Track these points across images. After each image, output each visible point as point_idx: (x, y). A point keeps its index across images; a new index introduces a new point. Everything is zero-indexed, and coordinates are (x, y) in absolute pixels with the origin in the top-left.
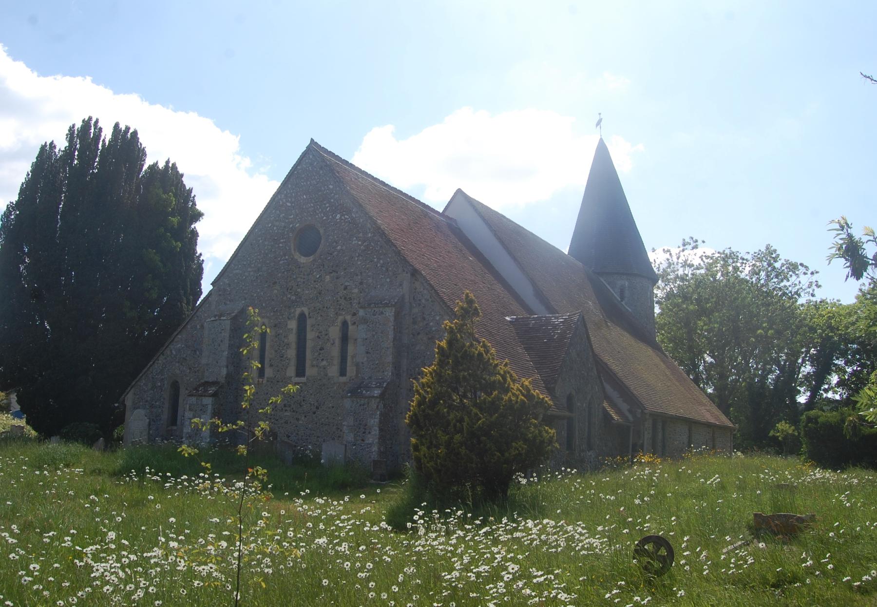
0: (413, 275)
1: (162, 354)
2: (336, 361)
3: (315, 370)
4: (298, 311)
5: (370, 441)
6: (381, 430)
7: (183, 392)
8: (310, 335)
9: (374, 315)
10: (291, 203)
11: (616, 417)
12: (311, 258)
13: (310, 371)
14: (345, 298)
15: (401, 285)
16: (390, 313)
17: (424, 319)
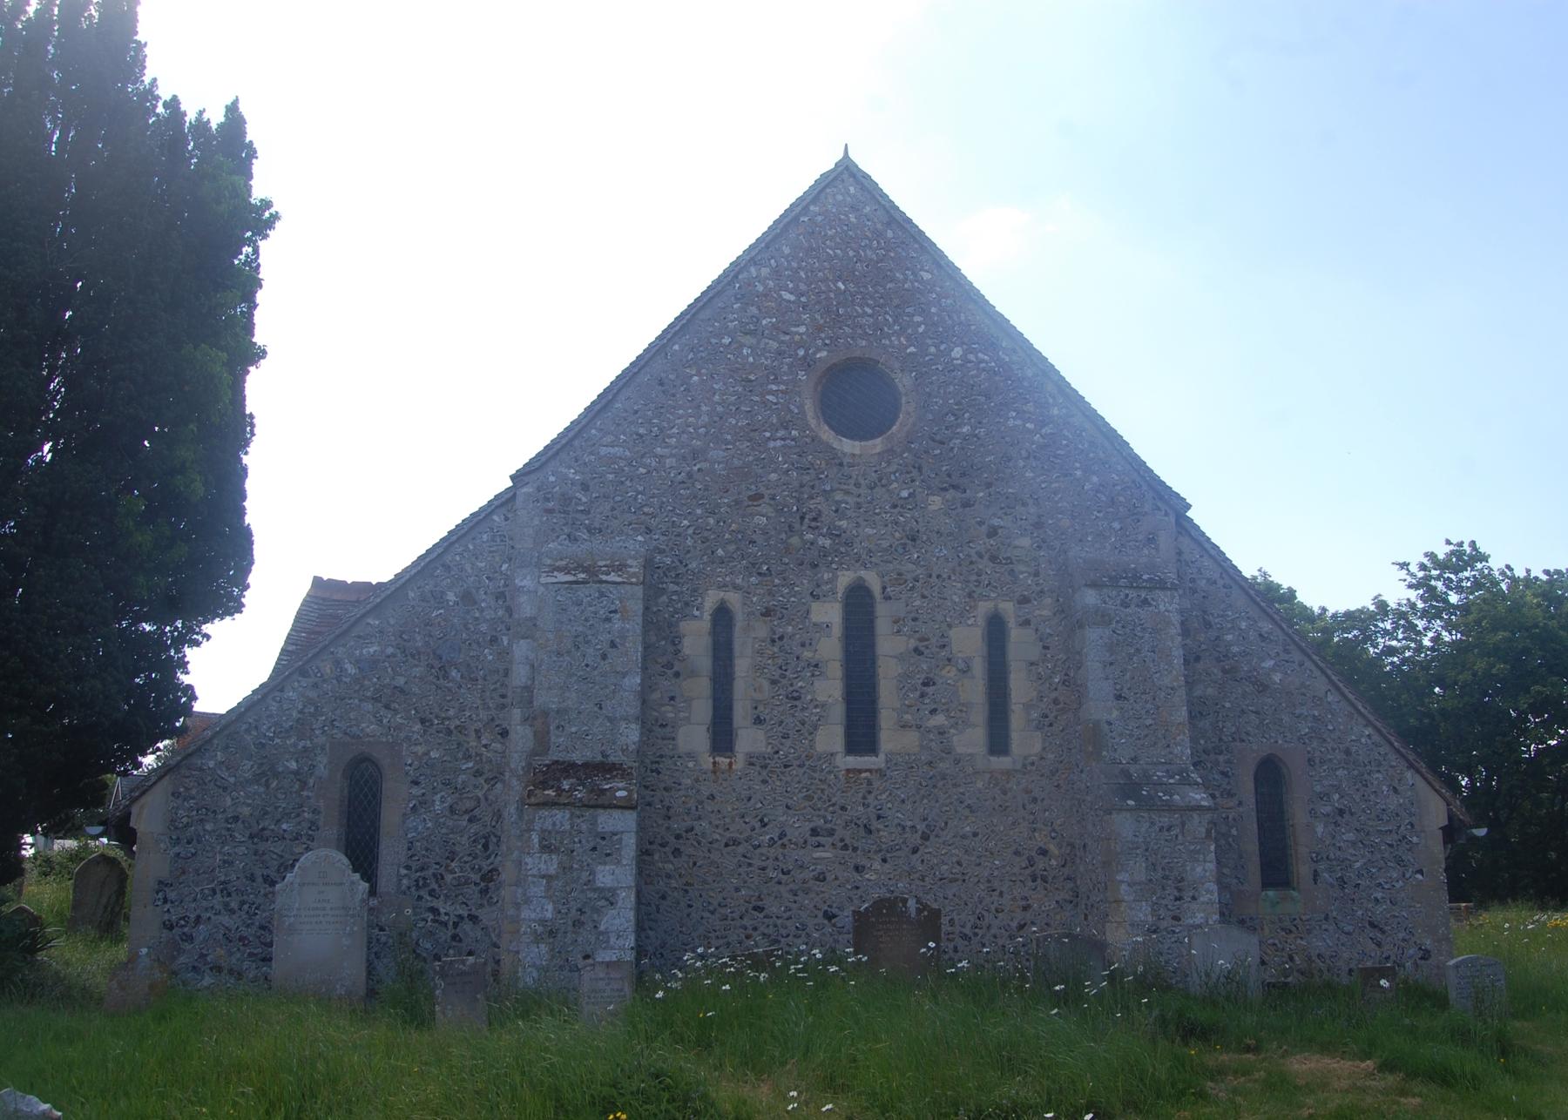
2: (979, 716)
3: (911, 740)
4: (845, 579)
5: (1199, 918)
8: (889, 646)
9: (1125, 605)
12: (878, 444)
13: (890, 739)
17: (1208, 625)
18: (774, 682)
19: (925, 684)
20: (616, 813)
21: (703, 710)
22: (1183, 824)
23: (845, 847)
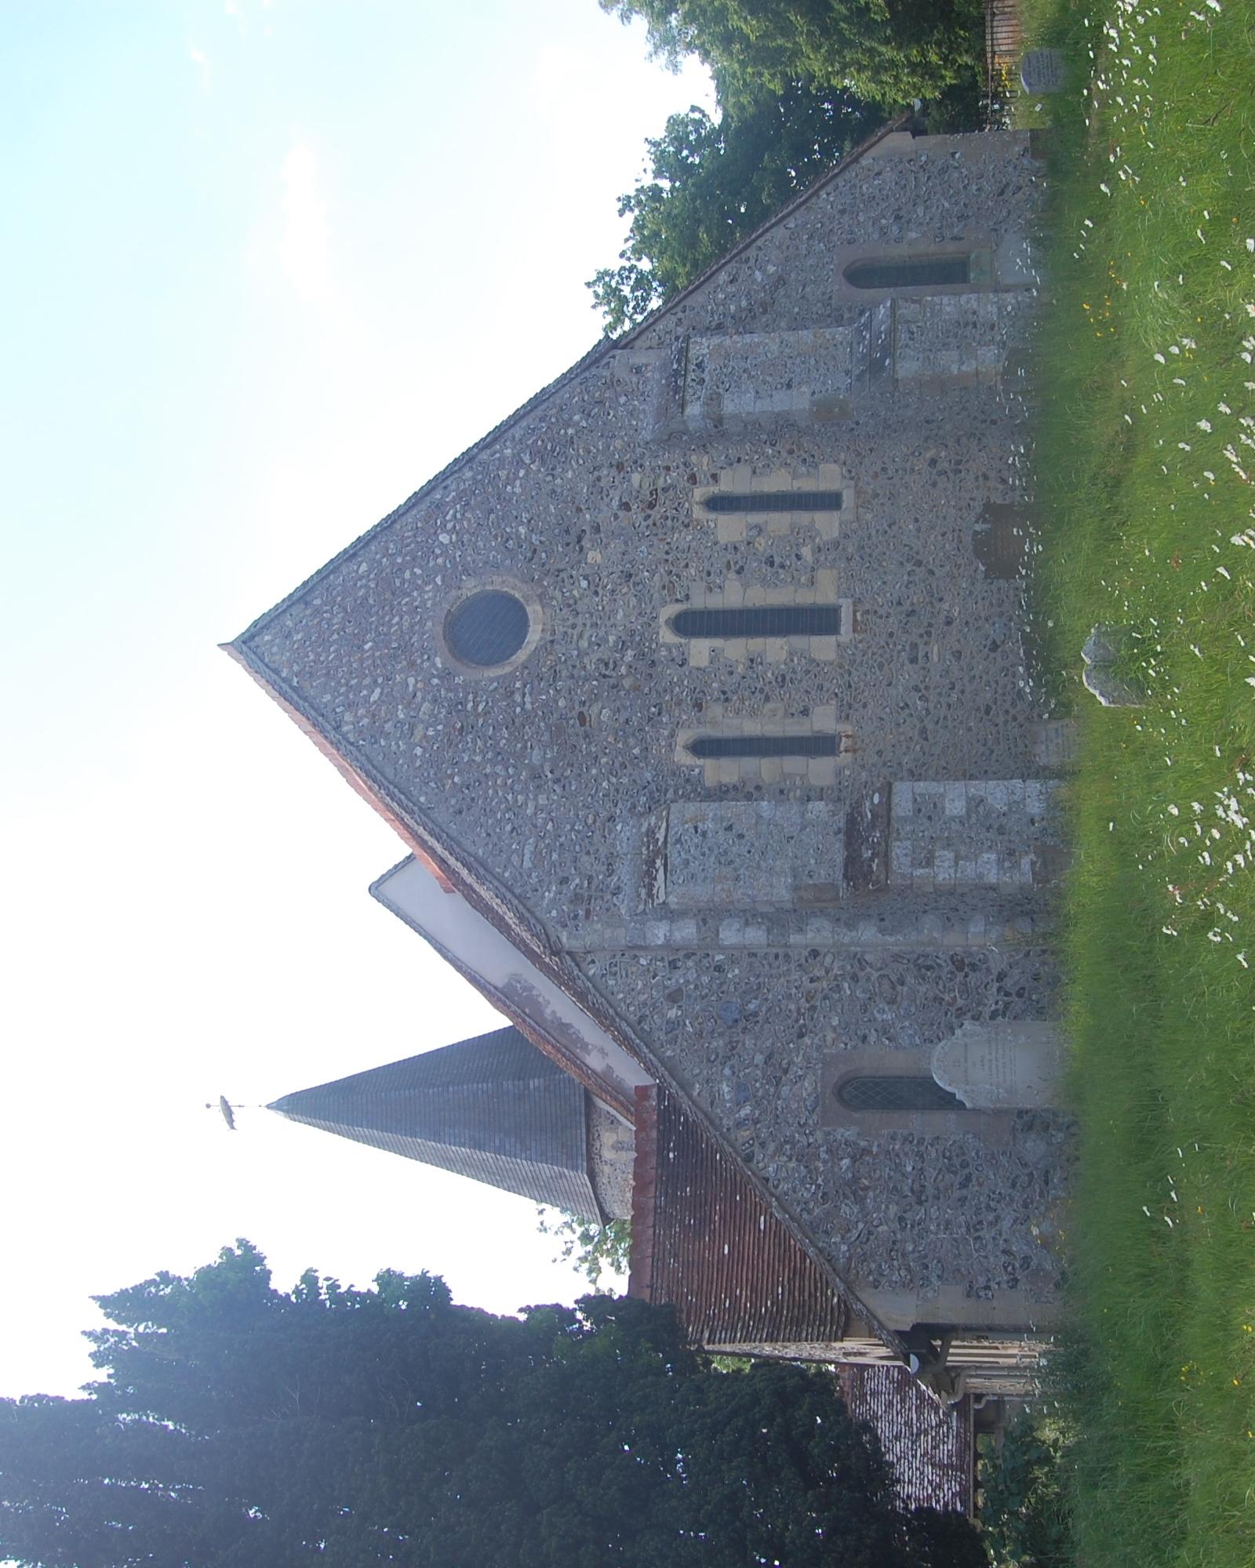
4: (667, 636)
13: (825, 592)
15: (638, 370)
18: (767, 699)
19: (772, 564)
20: (895, 799)
22: (907, 322)
23: (929, 634)
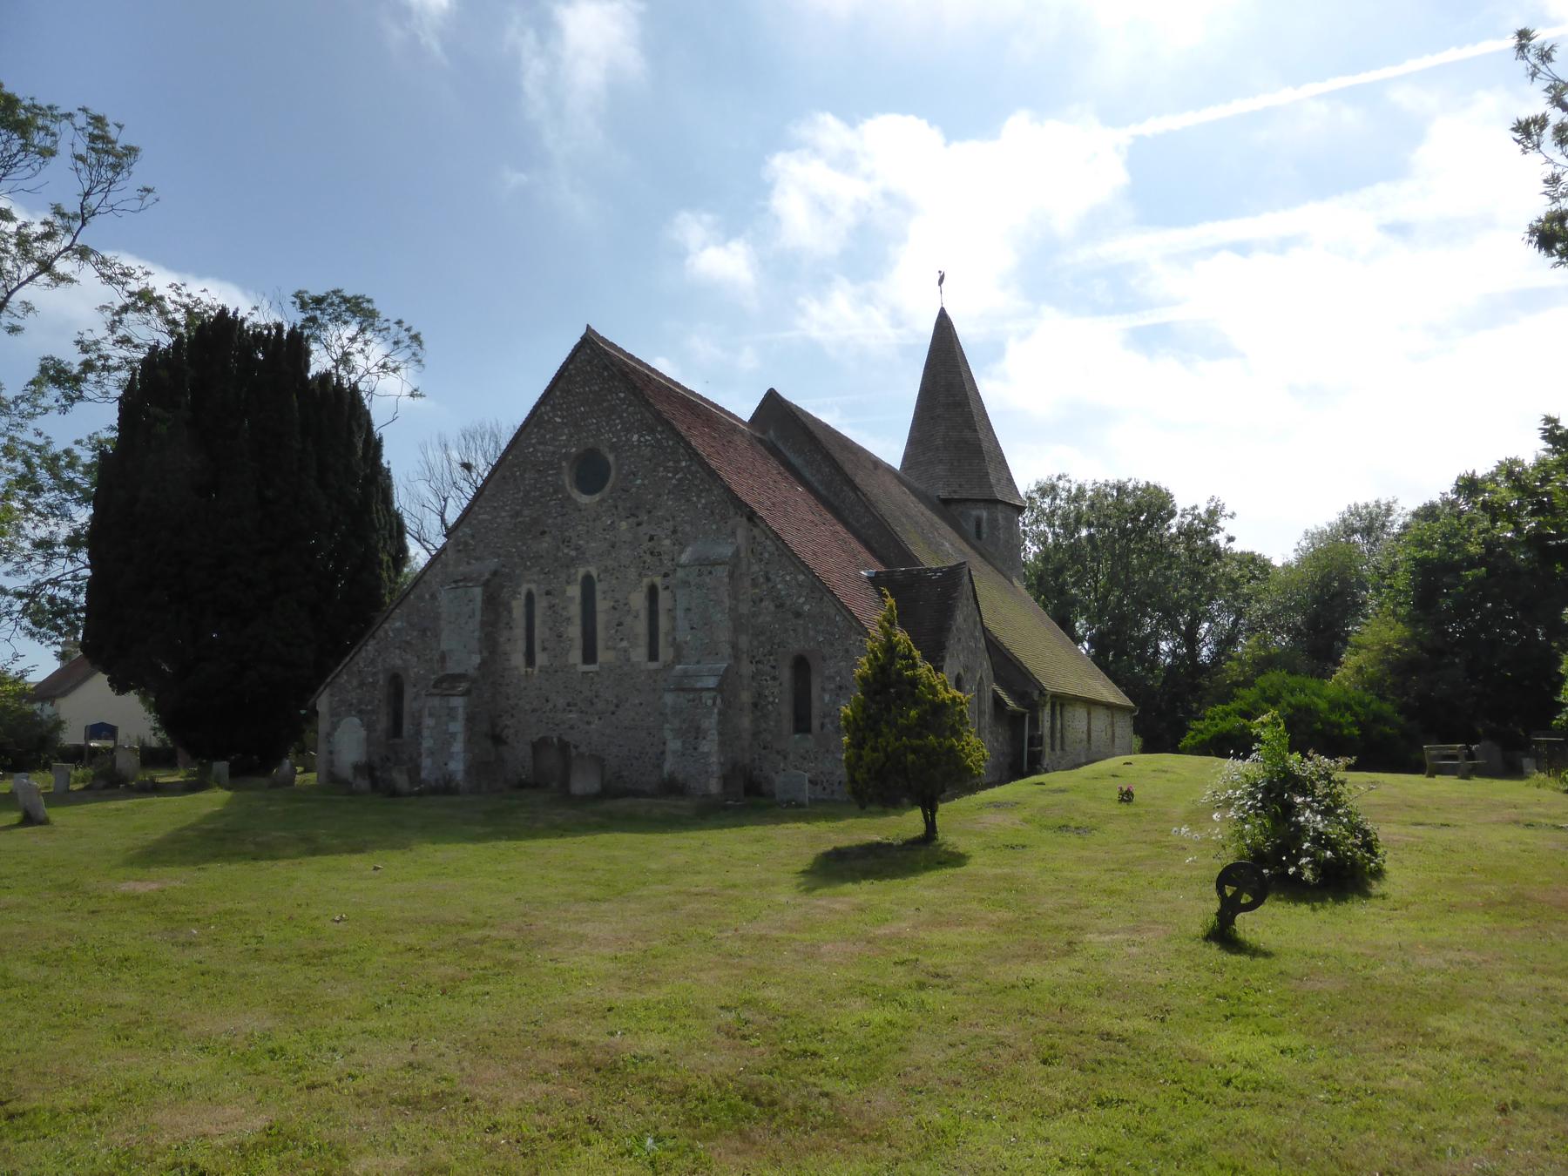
0: (750, 519)
1: (373, 636)
2: (643, 640)
4: (581, 572)
6: (720, 734)
7: (409, 692)
8: (602, 605)
10: (562, 417)
11: (1010, 703)
12: (597, 497)
13: (603, 656)
14: (652, 553)
16: (722, 572)
21: (521, 645)
